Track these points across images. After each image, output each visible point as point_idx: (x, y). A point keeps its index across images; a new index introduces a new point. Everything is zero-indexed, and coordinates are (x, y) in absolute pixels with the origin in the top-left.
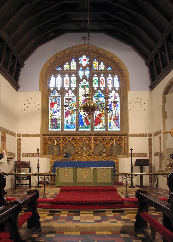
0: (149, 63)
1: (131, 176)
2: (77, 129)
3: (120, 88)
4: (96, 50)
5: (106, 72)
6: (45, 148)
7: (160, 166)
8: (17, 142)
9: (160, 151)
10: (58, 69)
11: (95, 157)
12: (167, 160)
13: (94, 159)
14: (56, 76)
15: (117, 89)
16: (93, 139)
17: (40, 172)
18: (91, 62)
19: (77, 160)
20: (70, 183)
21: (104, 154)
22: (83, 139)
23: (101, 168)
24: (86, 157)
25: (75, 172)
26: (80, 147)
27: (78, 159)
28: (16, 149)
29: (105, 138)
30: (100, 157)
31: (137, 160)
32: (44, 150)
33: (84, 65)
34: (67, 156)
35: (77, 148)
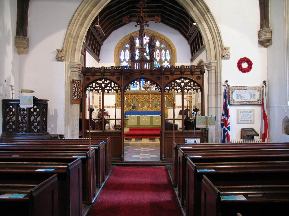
2: (140, 88)
3: (170, 60)
6: (118, 102)
10: (126, 46)
13: (152, 110)
14: (125, 51)
15: (168, 60)
16: (151, 96)
17: (116, 118)
19: (140, 110)
20: (149, 125)
21: (158, 106)
22: (144, 95)
24: (146, 108)
25: (138, 118)
26: (142, 101)
27: (140, 109)
28: (98, 103)
30: (156, 109)
34: (134, 107)
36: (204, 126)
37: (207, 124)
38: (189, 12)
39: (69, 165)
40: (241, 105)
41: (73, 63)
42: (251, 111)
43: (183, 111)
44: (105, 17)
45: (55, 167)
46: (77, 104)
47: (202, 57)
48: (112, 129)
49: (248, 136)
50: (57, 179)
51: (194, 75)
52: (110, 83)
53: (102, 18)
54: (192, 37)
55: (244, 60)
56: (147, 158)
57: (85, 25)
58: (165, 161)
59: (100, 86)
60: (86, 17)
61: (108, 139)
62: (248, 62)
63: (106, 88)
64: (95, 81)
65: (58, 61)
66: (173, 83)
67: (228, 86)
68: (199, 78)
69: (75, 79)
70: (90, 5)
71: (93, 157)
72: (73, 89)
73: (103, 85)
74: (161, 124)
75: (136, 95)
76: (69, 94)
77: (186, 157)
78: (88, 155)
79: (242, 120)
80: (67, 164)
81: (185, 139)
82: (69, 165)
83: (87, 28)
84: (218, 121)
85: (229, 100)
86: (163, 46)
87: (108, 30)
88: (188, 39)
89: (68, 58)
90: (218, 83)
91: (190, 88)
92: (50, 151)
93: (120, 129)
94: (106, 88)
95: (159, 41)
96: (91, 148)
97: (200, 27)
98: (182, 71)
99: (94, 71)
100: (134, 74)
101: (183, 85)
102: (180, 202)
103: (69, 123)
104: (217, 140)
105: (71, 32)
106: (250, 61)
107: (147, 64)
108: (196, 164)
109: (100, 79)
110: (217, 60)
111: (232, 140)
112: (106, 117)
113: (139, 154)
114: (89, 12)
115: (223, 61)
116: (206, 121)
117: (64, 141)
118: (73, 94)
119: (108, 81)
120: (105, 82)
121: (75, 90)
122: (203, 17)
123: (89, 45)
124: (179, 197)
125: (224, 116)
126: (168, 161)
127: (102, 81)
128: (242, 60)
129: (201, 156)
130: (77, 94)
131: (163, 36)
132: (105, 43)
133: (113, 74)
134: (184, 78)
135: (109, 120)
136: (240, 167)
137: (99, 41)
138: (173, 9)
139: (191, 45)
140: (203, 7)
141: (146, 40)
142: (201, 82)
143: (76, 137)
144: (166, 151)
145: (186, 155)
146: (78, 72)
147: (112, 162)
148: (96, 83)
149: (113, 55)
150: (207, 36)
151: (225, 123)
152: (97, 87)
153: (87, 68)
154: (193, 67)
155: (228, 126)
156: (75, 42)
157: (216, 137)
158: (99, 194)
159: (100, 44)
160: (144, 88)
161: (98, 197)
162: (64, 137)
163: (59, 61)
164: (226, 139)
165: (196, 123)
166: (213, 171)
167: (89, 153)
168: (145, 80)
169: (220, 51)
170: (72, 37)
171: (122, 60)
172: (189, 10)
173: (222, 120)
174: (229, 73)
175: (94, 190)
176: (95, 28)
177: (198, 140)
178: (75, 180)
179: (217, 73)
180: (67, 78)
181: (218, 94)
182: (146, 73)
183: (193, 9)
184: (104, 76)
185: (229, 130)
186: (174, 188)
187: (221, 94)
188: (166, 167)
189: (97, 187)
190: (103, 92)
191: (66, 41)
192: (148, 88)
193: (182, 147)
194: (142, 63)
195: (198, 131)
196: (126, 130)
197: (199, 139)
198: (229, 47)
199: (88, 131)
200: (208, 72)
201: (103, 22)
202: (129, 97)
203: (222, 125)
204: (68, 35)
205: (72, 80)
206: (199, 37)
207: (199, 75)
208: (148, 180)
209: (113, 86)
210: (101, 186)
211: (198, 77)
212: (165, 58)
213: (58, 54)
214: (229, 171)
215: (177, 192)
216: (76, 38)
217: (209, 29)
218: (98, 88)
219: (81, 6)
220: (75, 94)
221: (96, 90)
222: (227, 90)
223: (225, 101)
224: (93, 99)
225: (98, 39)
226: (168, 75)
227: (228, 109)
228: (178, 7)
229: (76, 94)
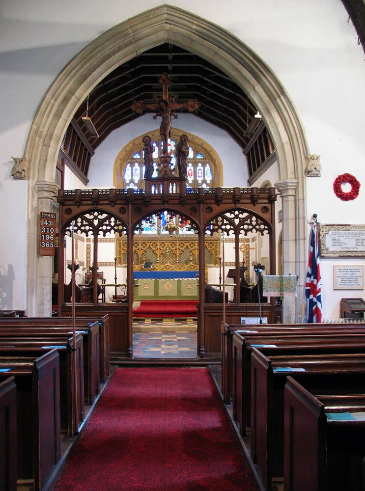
2: (159, 231)
3: (212, 181)
5: (195, 161)
8: (86, 248)
10: (135, 157)
14: (132, 165)
16: (177, 244)
17: (118, 283)
22: (166, 244)
25: (156, 285)
26: (162, 254)
27: (160, 268)
28: (86, 257)
30: (186, 267)
31: (230, 270)
34: (148, 265)
35: (159, 255)
36: (276, 294)
37: (283, 291)
38: (249, 93)
39: (37, 360)
40: (340, 257)
41: (44, 183)
42: (358, 268)
43: (237, 271)
44: (98, 105)
45: (12, 364)
46: (49, 257)
47: (269, 176)
48: (108, 301)
49: (353, 312)
50: (14, 385)
51: (257, 205)
52: (108, 218)
53: (93, 106)
54: (250, 142)
55: (346, 179)
56: (173, 354)
57: (64, 115)
58: (206, 358)
59: (90, 223)
60: (66, 100)
61: (105, 318)
62: (352, 181)
63: (101, 228)
64: (81, 215)
65: (15, 178)
66: (220, 219)
67: (318, 223)
68: (265, 209)
69: (46, 211)
71: (80, 349)
72: (42, 230)
73: (96, 222)
75: (151, 244)
76: (35, 237)
77: (248, 347)
78: (71, 344)
79: (342, 284)
80: (34, 359)
81: (242, 319)
82: (37, 360)
83: (67, 121)
84: (299, 286)
85: (320, 248)
86: (199, 158)
87: (104, 127)
88: (243, 146)
89: (34, 172)
90: (299, 218)
91: (250, 227)
93: (126, 301)
94: (101, 228)
95: (192, 148)
96: (76, 332)
97: (268, 120)
98: (235, 198)
99: (78, 198)
100: (151, 203)
101: (237, 221)
102: (237, 430)
103: (34, 290)
104: (298, 320)
105: (38, 128)
106: (356, 181)
107: (175, 185)
108: (270, 357)
109: (90, 212)
110: (298, 178)
111: (324, 320)
112: (100, 282)
113: (159, 346)
114: (71, 93)
115: (310, 181)
116: (281, 285)
117: (26, 322)
118: (41, 238)
119: (105, 215)
120: (100, 217)
121: (46, 230)
122: (273, 104)
123: (70, 154)
124: (236, 420)
125: (310, 277)
126: (212, 358)
127: (93, 215)
128: (342, 178)
129: (274, 346)
130: (49, 237)
131: (201, 140)
132: (98, 151)
133: (113, 203)
134: (238, 210)
135: (105, 286)
136: (351, 364)
137: (87, 147)
138: (216, 92)
139: (248, 155)
140: (274, 84)
141: (172, 146)
142: (270, 217)
143: (48, 313)
144: (208, 340)
145: (248, 344)
146: (51, 199)
147: (112, 360)
148: (84, 219)
149: (113, 170)
150: (279, 134)
151: (312, 290)
152: (85, 226)
153: (68, 192)
154: (255, 191)
155: (319, 294)
156: (46, 146)
157: (295, 314)
158: (89, 417)
159: (89, 154)
160: (167, 229)
161: (88, 422)
162: (26, 314)
163: (18, 179)
164: (315, 318)
165: (263, 287)
166: (302, 370)
167: (73, 340)
168: (171, 214)
169: (304, 161)
170: (40, 137)
171: (128, 182)
172: (248, 91)
173: (307, 285)
174: (319, 201)
175: (82, 410)
176: (82, 123)
177: (265, 320)
178: (47, 391)
179: (299, 201)
181: (299, 238)
182: (171, 201)
183: (256, 88)
184: (98, 206)
185: (320, 301)
186: (226, 405)
187: (304, 239)
188: (208, 368)
189: (86, 404)
190: (96, 234)
191: (30, 143)
192: (174, 229)
193: (238, 331)
194: (166, 182)
195: (265, 304)
196: (136, 305)
197: (266, 318)
198: (320, 156)
199: (68, 304)
200: (282, 200)
201: (96, 113)
202: (140, 247)
203: (308, 293)
204: (34, 134)
205: (40, 213)
206: (263, 141)
207: (265, 205)
208: (176, 391)
209: (113, 224)
210: (94, 401)
212: (202, 178)
213: (16, 166)
214: (330, 371)
215: (230, 412)
216: (48, 138)
217: (283, 124)
219: (56, 82)
220: (45, 238)
222: (315, 230)
223: (312, 251)
224: (78, 247)
225: (85, 144)
226: (211, 204)
227: (317, 264)
228: (226, 89)
229: (48, 237)
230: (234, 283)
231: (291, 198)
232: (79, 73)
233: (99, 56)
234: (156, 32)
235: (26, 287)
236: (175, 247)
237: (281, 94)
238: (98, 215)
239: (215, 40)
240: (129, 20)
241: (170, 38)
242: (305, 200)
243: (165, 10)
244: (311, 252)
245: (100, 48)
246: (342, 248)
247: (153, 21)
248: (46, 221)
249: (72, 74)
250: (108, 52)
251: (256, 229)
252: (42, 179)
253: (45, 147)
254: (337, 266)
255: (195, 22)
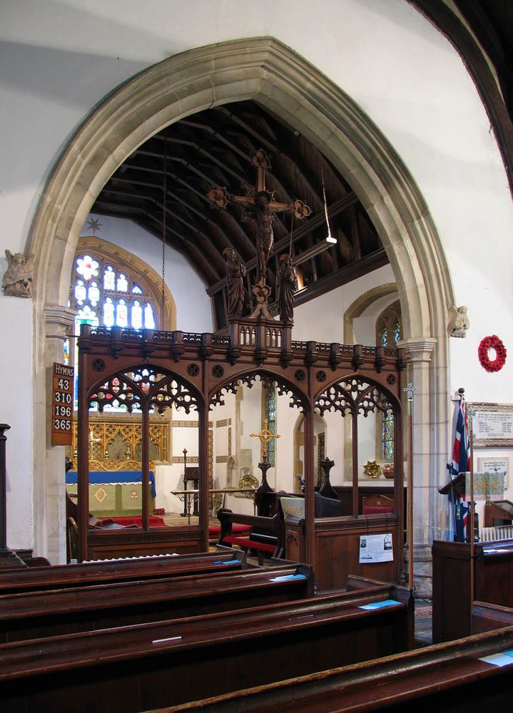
0: (215, 292)
1: (183, 495)
4: (117, 253)
5: (131, 297)
7: (229, 480)
9: (230, 454)
11: (112, 463)
12: (242, 469)
18: (102, 270)
20: (111, 511)
23: (131, 483)
29: (127, 427)
30: (122, 464)
32: (98, 444)
33: (87, 277)
38: (372, 205)
42: (504, 461)
51: (237, 365)
59: (348, 397)
70: (117, 123)
74: (141, 508)
81: (362, 538)
91: (328, 403)
92: (331, 605)
100: (182, 356)
101: (354, 395)
104: (436, 533)
105: (54, 201)
109: (136, 369)
110: (437, 337)
114: (108, 148)
115: (453, 342)
122: (406, 227)
127: (141, 374)
134: (149, 367)
148: (123, 380)
153: (296, 344)
170: (54, 221)
171: (80, 303)
172: (372, 202)
174: (462, 369)
179: (437, 370)
180: (40, 356)
182: (269, 360)
187: (446, 422)
197: (391, 535)
211: (193, 366)
216: (64, 224)
218: (343, 403)
220: (60, 412)
221: (336, 406)
230: (196, 488)
231: (425, 365)
232: (124, 116)
233: (159, 95)
234: (247, 78)
235: (32, 504)
236: (130, 434)
237: (422, 214)
238: (149, 375)
239: (335, 113)
240: (218, 45)
241: (265, 93)
242: (448, 369)
243: (268, 46)
244: (456, 440)
245: (164, 80)
246: (489, 435)
247: (248, 58)
248: (62, 380)
249: (115, 115)
250: (172, 90)
251: (177, 401)
252: (53, 301)
253: (57, 241)
254: (483, 459)
255: (312, 79)
